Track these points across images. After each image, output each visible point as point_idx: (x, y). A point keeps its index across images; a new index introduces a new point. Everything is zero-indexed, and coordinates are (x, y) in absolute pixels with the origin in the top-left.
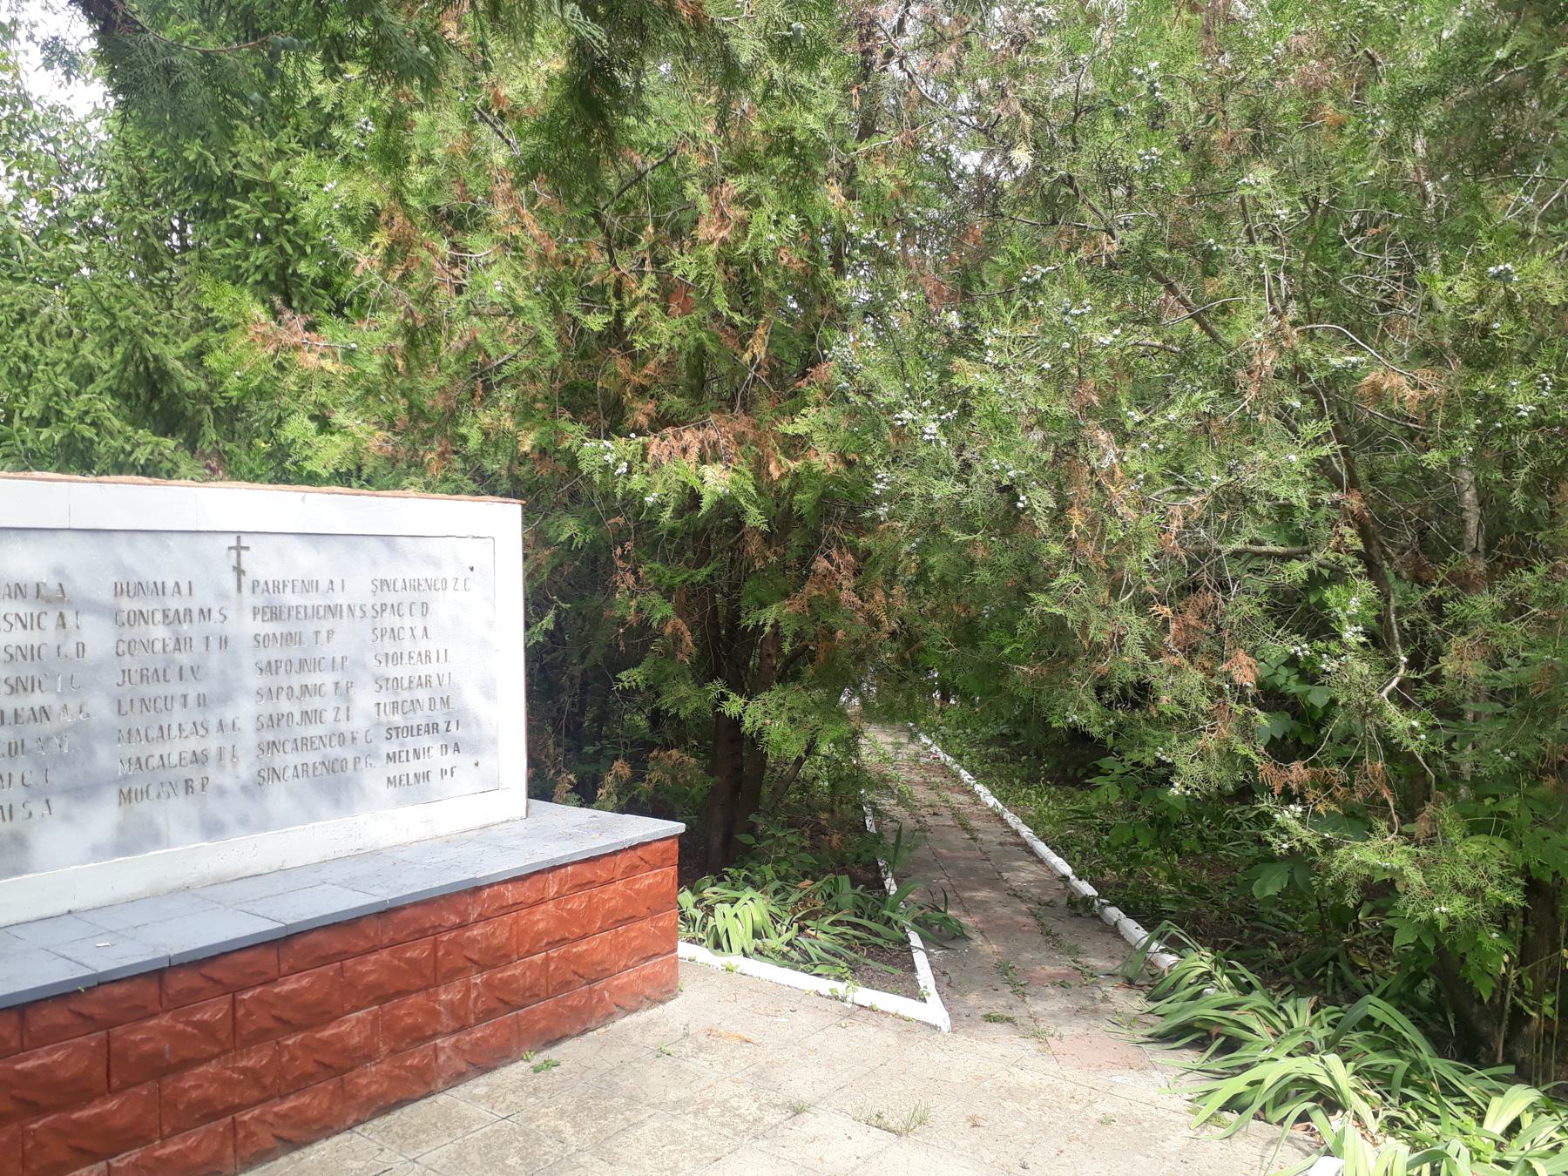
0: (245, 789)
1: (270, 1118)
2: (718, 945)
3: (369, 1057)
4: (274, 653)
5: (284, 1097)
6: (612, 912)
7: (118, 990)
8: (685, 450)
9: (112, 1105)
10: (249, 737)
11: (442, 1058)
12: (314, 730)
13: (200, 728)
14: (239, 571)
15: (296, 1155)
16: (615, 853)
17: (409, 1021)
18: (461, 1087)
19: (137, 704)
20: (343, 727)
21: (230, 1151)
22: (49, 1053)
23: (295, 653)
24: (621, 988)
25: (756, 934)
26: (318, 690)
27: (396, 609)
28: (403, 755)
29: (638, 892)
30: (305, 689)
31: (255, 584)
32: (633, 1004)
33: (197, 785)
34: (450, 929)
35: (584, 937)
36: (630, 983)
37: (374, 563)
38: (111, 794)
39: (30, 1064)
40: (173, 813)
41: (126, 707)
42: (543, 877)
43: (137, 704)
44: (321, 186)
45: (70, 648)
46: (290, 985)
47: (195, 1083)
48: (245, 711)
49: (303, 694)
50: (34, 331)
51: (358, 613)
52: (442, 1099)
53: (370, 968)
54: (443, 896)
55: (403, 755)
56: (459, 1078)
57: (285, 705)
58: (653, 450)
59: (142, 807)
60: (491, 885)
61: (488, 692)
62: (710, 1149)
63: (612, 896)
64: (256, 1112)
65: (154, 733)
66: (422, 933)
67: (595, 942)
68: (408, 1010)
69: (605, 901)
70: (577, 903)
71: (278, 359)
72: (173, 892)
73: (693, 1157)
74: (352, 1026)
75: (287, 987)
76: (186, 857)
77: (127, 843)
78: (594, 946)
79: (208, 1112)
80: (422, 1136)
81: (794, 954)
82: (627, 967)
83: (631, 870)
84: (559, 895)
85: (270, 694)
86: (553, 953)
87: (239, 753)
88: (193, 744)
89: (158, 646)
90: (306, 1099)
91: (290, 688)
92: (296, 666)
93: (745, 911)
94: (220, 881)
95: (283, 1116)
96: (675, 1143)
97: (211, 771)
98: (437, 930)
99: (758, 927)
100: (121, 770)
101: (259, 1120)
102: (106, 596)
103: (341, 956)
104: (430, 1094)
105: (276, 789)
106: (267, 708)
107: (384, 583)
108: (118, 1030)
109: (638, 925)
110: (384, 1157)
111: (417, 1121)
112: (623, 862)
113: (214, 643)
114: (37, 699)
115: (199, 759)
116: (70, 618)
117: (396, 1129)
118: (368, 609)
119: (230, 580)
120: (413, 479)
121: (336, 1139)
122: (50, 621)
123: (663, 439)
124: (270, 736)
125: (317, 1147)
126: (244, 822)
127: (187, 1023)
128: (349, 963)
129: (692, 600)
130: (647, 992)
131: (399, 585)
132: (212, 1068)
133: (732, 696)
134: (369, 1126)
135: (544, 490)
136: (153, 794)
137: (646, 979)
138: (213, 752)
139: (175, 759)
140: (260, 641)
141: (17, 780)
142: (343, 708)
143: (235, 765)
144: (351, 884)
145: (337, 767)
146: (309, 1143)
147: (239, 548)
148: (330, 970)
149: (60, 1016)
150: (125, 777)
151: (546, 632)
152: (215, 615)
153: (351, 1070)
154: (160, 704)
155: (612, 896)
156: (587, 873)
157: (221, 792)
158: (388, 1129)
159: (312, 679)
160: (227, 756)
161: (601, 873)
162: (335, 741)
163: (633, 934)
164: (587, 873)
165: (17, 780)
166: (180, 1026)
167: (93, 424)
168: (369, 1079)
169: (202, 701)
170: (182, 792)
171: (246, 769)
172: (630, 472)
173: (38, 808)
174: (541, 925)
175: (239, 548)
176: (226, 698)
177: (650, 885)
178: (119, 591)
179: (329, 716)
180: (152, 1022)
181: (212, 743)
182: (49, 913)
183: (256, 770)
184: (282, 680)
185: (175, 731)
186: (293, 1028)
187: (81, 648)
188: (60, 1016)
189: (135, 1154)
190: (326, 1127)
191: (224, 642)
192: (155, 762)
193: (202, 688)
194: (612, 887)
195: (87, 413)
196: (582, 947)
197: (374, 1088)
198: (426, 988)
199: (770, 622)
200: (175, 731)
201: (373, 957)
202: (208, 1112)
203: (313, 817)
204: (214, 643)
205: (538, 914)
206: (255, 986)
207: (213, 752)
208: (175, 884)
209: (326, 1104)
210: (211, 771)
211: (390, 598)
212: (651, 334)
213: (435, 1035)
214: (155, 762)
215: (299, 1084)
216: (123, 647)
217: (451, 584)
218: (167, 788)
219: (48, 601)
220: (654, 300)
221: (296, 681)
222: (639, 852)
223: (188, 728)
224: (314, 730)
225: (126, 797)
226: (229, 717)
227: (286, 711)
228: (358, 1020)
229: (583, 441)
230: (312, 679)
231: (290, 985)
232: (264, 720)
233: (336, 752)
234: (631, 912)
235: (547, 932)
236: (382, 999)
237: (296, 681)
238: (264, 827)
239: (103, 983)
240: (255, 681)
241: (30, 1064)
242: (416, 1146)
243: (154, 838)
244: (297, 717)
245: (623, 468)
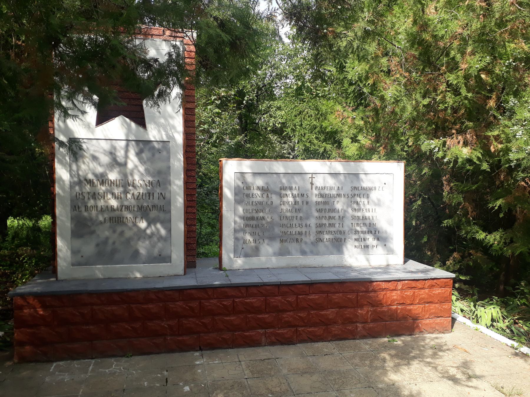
0: (312, 243)
1: (306, 331)
2: (477, 322)
3: (335, 323)
4: (321, 207)
5: (310, 327)
6: (423, 299)
7: (268, 288)
8: (459, 142)
9: (267, 316)
10: (314, 229)
11: (359, 329)
12: (332, 229)
13: (300, 225)
14: (312, 184)
15: (313, 344)
16: (425, 280)
17: (348, 316)
18: (365, 340)
19: (285, 218)
20: (341, 229)
21: (295, 337)
22: (252, 299)
23: (327, 207)
24: (427, 324)
25: (493, 320)
26: (334, 218)
27: (359, 196)
28: (360, 240)
29: (434, 294)
30: (330, 217)
31: (316, 187)
32: (431, 331)
33: (299, 240)
34: (362, 292)
35: (411, 304)
36: (431, 324)
37: (352, 182)
38: (278, 240)
39: (248, 301)
40: (293, 247)
41: (282, 218)
42: (396, 282)
43: (285, 218)
44: (353, 68)
45: (269, 203)
46: (312, 297)
47: (287, 316)
48: (313, 222)
49: (329, 219)
50: (303, 116)
51: (346, 196)
52: (357, 341)
53: (336, 297)
54: (360, 282)
55: (360, 240)
56: (363, 337)
57: (324, 221)
58: (448, 143)
59: (285, 244)
60: (377, 281)
61: (390, 223)
62: (431, 378)
63: (424, 293)
64: (303, 329)
65: (289, 225)
66: (353, 291)
67: (416, 307)
68: (348, 312)
69: (420, 295)
70: (409, 293)
71: (343, 121)
72: (292, 267)
73: (423, 379)
74: (330, 313)
75: (311, 297)
76: (297, 259)
77: (282, 253)
78: (416, 309)
79: (289, 325)
80: (347, 349)
81: (508, 331)
82: (429, 318)
83: (431, 287)
84: (402, 289)
85: (319, 218)
86: (399, 307)
87: (311, 233)
88: (298, 229)
89: (290, 203)
90: (316, 329)
91: (326, 217)
92: (327, 211)
93: (490, 311)
94: (305, 267)
95: (310, 332)
96: (420, 373)
97: (303, 237)
98: (358, 292)
99: (494, 317)
100: (281, 234)
101: (303, 330)
102: (278, 190)
103: (328, 292)
104: (354, 339)
105: (321, 244)
106: (319, 222)
107: (355, 188)
108: (268, 298)
109: (434, 305)
110: (334, 351)
111: (347, 344)
112: (428, 283)
113: (305, 203)
114: (261, 215)
115: (300, 233)
116: (270, 195)
117: (341, 345)
118: (350, 195)
119: (310, 186)
120: (376, 156)
121: (324, 343)
122: (265, 196)
123: (452, 139)
124: (319, 229)
125: (319, 343)
126: (312, 253)
127: (285, 300)
128: (329, 295)
129: (468, 195)
130: (437, 328)
131: (360, 188)
132: (291, 313)
133: (481, 232)
134: (334, 342)
135: (414, 158)
136: (288, 241)
137: (437, 324)
138: (304, 232)
139: (294, 233)
140: (317, 203)
141: (257, 234)
142: (341, 224)
143: (309, 236)
144: (335, 274)
145: (339, 240)
146: (317, 342)
147: (312, 178)
148: (324, 295)
149: (255, 291)
150: (282, 236)
151: (419, 205)
152: (305, 195)
153: (330, 325)
154: (290, 218)
155: (424, 293)
156: (414, 284)
157: (306, 243)
158: (339, 344)
159: (332, 215)
160: (308, 234)
161: (419, 285)
162: (338, 233)
163: (431, 308)
164: (414, 284)
165: (257, 234)
166: (283, 300)
167: (310, 142)
168: (335, 329)
169: (301, 218)
170: (295, 242)
171: (312, 238)
172: (439, 151)
173: (261, 241)
174: (395, 297)
175: (312, 178)
176: (308, 218)
177: (439, 293)
178: (281, 189)
179: (337, 225)
180: (277, 298)
181: (304, 230)
182: (263, 267)
183: (315, 238)
184: (323, 214)
185: (294, 226)
186: (314, 309)
187: (272, 202)
188: (255, 291)
189: (271, 330)
190: (322, 339)
191: (307, 203)
192: (289, 233)
193: (301, 215)
194: (423, 291)
195: (308, 139)
196: (411, 307)
197: (336, 332)
198: (354, 308)
199: (498, 205)
200: (294, 226)
201: (337, 295)
202: (289, 325)
203: (332, 254)
204: (305, 203)
205: (394, 293)
206: (303, 295)
207: (304, 232)
208: (293, 266)
209: (322, 332)
210: (303, 237)
211: (357, 192)
212: (446, 103)
213: (357, 322)
214: (289, 233)
215: (315, 325)
216: (282, 203)
217: (377, 188)
218: (292, 240)
219: (265, 191)
220: (448, 91)
221: (327, 215)
222: (435, 281)
223: (297, 225)
224: (332, 229)
225: (282, 241)
226: (308, 223)
227: (324, 223)
228: (332, 312)
229: (425, 141)
230: (332, 215)
231: (312, 297)
232: (318, 225)
233: (339, 236)
234: (430, 300)
235: (396, 300)
236: (341, 307)
237: (327, 215)
238: (317, 254)
239: (264, 285)
240: (316, 214)
241: (248, 301)
242: (343, 351)
243: (289, 253)
244: (327, 225)
245: (437, 149)
